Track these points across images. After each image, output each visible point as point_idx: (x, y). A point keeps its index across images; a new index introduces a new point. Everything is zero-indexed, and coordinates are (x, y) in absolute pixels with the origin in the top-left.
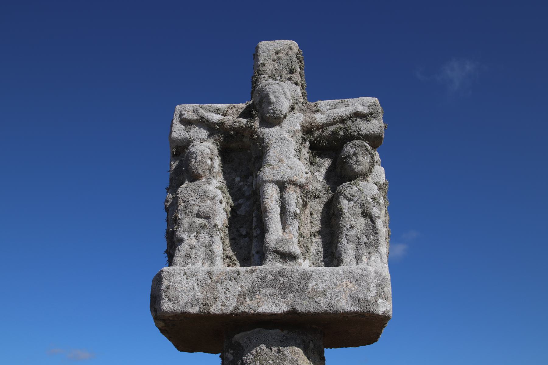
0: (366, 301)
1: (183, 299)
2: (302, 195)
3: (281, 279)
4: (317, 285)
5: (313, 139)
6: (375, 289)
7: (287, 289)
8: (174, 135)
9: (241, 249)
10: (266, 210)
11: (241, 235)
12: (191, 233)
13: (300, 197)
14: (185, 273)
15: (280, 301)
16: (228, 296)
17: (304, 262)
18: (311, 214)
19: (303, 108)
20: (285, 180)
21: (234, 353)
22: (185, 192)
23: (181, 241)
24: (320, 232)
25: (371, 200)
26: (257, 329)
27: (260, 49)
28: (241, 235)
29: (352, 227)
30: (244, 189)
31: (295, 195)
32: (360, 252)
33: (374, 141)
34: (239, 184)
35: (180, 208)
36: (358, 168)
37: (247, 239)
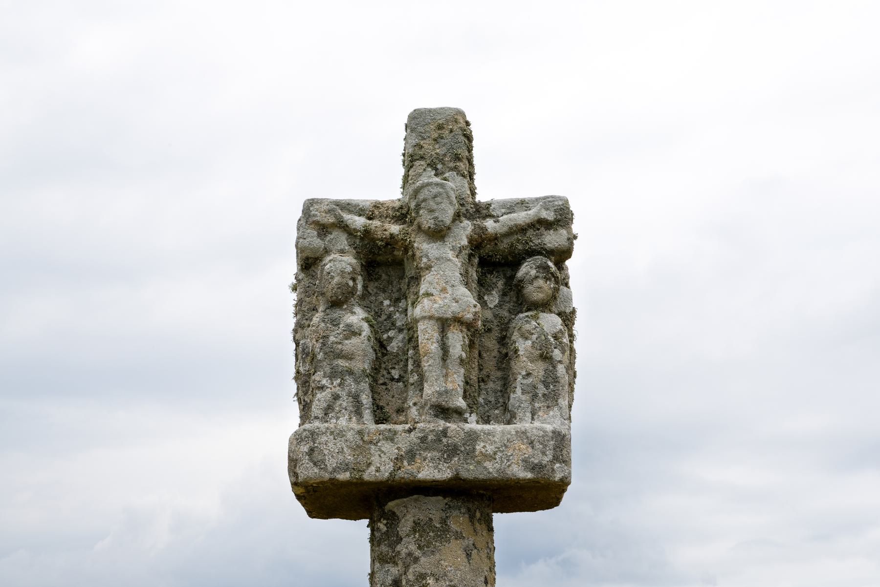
4: (484, 447)
7: (452, 451)
9: (393, 397)
12: (333, 379)
13: (466, 337)
15: (443, 466)
16: (383, 460)
17: (470, 416)
18: (480, 355)
21: (387, 523)
25: (552, 340)
26: (415, 496)
29: (529, 375)
30: (394, 317)
33: (561, 256)
34: (388, 309)
37: (401, 384)
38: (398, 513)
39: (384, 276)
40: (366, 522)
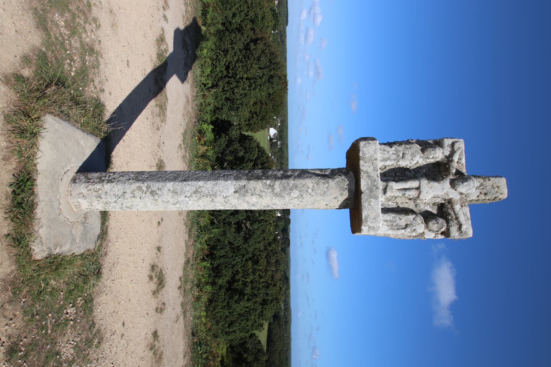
0: (367, 221)
1: (365, 150)
2: (415, 197)
3: (375, 188)
4: (373, 202)
5: (446, 204)
6: (372, 226)
8: (446, 140)
10: (406, 182)
11: (396, 173)
14: (376, 150)
15: (366, 187)
19: (463, 199)
20: (421, 189)
22: (415, 147)
23: (391, 147)
24: (398, 207)
25: (414, 228)
26: (355, 180)
27: (500, 179)
28: (396, 173)
29: (400, 219)
31: (414, 194)
32: (389, 222)
35: (407, 146)
36: (430, 224)
37: (394, 175)
38: (349, 175)
39: (435, 170)
40: (344, 166)
